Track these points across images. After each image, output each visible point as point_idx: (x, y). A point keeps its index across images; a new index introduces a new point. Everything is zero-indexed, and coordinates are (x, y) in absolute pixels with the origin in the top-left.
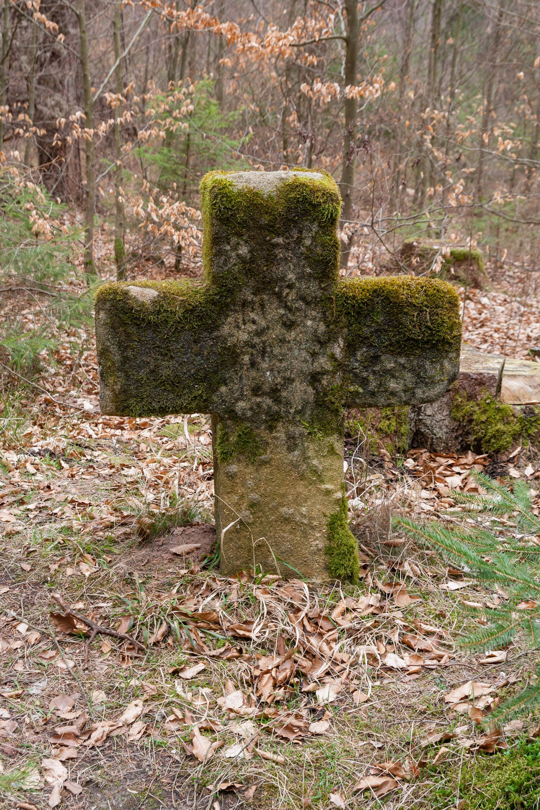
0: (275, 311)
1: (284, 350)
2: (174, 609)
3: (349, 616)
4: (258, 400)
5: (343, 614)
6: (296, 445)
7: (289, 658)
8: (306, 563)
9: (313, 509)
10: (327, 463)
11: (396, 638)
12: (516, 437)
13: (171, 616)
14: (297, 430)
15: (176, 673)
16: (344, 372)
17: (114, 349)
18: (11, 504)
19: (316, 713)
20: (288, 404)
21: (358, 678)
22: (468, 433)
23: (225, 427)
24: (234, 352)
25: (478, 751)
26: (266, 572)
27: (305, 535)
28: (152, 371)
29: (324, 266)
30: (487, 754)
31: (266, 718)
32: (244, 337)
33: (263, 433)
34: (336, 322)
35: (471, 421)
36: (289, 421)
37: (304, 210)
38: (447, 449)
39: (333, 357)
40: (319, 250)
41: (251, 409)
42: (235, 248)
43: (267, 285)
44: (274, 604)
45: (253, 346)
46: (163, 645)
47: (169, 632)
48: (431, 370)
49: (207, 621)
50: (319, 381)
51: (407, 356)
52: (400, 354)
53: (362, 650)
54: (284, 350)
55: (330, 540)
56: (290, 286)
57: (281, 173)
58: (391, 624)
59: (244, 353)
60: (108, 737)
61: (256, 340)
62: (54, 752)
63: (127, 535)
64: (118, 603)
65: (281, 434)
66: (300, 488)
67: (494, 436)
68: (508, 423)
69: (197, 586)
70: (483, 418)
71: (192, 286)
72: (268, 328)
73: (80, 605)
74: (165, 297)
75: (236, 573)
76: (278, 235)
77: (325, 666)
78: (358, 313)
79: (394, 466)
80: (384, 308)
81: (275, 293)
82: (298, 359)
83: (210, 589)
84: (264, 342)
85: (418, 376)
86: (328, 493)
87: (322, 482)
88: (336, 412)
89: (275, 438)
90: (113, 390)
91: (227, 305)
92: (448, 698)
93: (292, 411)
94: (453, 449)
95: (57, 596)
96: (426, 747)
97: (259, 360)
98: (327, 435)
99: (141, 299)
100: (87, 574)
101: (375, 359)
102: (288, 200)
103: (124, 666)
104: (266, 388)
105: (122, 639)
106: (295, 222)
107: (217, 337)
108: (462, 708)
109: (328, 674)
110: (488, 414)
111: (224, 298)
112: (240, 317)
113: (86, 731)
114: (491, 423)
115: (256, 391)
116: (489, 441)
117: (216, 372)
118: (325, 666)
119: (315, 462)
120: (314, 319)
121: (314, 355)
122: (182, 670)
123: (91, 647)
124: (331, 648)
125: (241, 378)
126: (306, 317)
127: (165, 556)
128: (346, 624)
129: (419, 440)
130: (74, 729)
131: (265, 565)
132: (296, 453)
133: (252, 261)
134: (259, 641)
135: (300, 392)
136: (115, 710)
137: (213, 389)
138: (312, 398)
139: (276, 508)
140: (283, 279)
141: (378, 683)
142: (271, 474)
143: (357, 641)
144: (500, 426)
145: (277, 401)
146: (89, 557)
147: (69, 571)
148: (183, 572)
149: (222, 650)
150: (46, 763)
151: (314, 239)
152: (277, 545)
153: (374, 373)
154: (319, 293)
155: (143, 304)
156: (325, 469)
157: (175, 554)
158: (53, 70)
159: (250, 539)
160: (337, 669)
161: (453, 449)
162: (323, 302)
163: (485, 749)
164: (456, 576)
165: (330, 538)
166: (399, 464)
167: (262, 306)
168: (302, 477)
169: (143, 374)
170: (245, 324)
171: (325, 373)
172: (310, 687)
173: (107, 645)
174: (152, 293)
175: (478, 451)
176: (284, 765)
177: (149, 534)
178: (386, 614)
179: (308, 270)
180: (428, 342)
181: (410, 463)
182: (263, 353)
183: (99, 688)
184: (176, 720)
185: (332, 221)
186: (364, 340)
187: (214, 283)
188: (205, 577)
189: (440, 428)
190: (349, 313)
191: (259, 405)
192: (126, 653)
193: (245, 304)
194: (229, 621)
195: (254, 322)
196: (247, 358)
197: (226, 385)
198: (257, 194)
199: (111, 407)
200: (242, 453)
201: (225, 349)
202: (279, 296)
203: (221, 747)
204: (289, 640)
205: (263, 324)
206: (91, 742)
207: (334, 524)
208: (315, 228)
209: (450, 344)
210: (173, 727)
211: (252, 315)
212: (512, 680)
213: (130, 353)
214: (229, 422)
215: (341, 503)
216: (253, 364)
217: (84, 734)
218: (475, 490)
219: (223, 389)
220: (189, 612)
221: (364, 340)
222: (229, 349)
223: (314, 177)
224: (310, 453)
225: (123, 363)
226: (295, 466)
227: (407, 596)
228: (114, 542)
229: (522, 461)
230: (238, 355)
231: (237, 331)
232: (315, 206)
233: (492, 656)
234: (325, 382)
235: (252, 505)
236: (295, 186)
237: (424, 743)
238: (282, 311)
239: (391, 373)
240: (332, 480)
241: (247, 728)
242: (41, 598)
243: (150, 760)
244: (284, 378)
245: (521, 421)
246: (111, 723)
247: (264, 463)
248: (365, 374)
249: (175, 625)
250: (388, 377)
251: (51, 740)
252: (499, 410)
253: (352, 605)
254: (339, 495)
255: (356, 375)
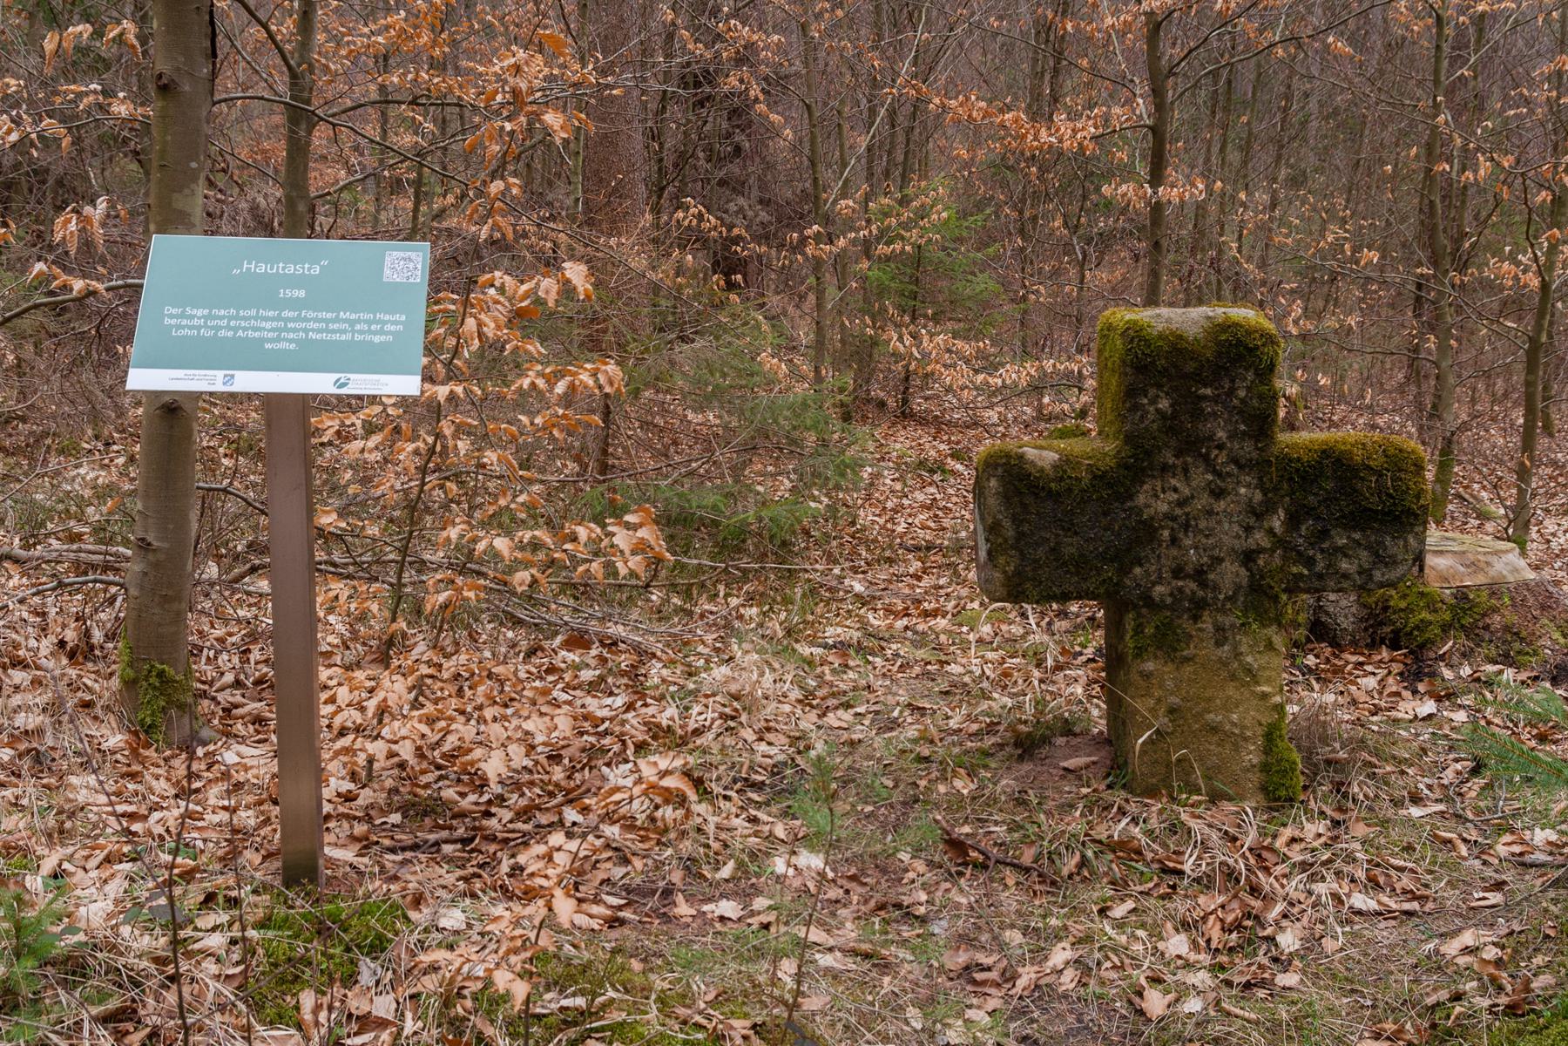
0: (1202, 477)
1: (1213, 523)
2: (1086, 835)
3: (1297, 847)
4: (1180, 583)
5: (1288, 845)
6: (1226, 639)
7: (1235, 896)
8: (1236, 783)
9: (1245, 716)
10: (1264, 660)
11: (1360, 875)
12: (1446, 628)
13: (1083, 844)
14: (1227, 621)
15: (1103, 912)
16: (1285, 549)
17: (1007, 523)
18: (836, 708)
19: (1282, 962)
20: (1216, 588)
21: (1322, 922)
22: (1381, 624)
23: (1139, 615)
24: (1151, 526)
25: (1505, 1013)
26: (1190, 793)
27: (1236, 748)
28: (1053, 550)
29: (1261, 423)
30: (1516, 1015)
31: (1222, 968)
32: (1164, 508)
33: (1185, 623)
34: (1276, 489)
35: (1386, 608)
36: (1218, 610)
37: (1239, 355)
38: (1354, 643)
39: (1271, 531)
40: (1255, 403)
41: (1171, 594)
42: (1153, 402)
43: (1193, 446)
44: (1207, 830)
45: (1174, 519)
46: (1078, 879)
47: (1084, 862)
48: (1392, 546)
49: (1126, 850)
50: (1255, 561)
51: (1363, 530)
52: (1354, 528)
53: (1320, 888)
54: (1213, 523)
55: (1266, 753)
56: (1220, 447)
57: (1219, 312)
58: (1351, 859)
59: (1163, 528)
60: (1037, 987)
61: (1178, 511)
62: (975, 1001)
63: (1001, 746)
64: (1014, 827)
65: (1207, 624)
66: (1231, 691)
67: (1417, 627)
68: (1435, 611)
69: (1105, 809)
70: (1403, 605)
71: (1097, 445)
72: (1193, 497)
73: (967, 829)
74: (1068, 461)
75: (1152, 792)
76: (1205, 386)
77: (1279, 908)
78: (1303, 478)
79: (1293, 665)
80: (1335, 471)
81: (1201, 455)
82: (1229, 534)
83: (1122, 812)
84: (1187, 514)
85: (1377, 555)
86: (1265, 696)
87: (1257, 683)
88: (1276, 599)
89: (1200, 630)
90: (1005, 572)
91: (1143, 470)
92: (1443, 949)
93: (1221, 597)
94: (1362, 644)
95: (939, 817)
96: (1433, 1007)
97: (1181, 535)
98: (1264, 626)
99: (1040, 464)
100: (965, 792)
101: (1324, 534)
102: (1219, 343)
103: (1037, 902)
104: (1189, 569)
105: (1027, 870)
106: (1227, 369)
107: (1131, 508)
108: (1463, 961)
109: (1285, 916)
110: (1409, 599)
111: (1139, 462)
112: (1159, 484)
113: (1010, 977)
114: (1412, 611)
115: (1178, 572)
116: (1411, 633)
117: (1129, 550)
118: (1279, 908)
119: (1249, 659)
120: (1248, 486)
121: (1248, 529)
122: (1108, 908)
123: (992, 880)
124: (1283, 886)
125: (1159, 557)
126: (1238, 483)
127: (1054, 772)
128: (1297, 856)
129: (1321, 631)
130: (994, 975)
131: (1187, 784)
132: (1226, 648)
133: (1174, 416)
134: (1194, 875)
135: (1231, 574)
136: (1039, 955)
137: (1124, 571)
138: (1245, 582)
139: (1201, 715)
140: (1211, 438)
141: (1347, 929)
142: (1195, 673)
143: (1313, 878)
144: (1425, 615)
145: (1203, 584)
146: (962, 771)
147: (942, 789)
148: (1085, 791)
149: (1151, 885)
150: (970, 1014)
151: (1249, 389)
152: (1201, 759)
153: (1322, 551)
154: (1255, 455)
155: (1042, 470)
156: (1262, 668)
157: (1065, 769)
158: (734, 168)
159: (1168, 752)
160: (1295, 910)
161: (1362, 644)
162: (1259, 466)
163: (1512, 1010)
164: (1416, 799)
165: (1267, 751)
166: (1298, 661)
167: (1186, 471)
168: (1233, 677)
169: (1041, 552)
170: (1164, 492)
171: (1260, 551)
172: (1269, 931)
173: (1011, 878)
174: (1051, 457)
175: (1394, 646)
176: (1257, 1023)
177: (1027, 745)
178: (1344, 846)
179: (1243, 427)
180: (1390, 512)
181: (1311, 660)
182: (1186, 527)
183: (1012, 926)
184: (1114, 967)
185: (1272, 367)
186: (1310, 511)
187: (1126, 443)
188: (1118, 797)
189: (1346, 617)
190: (1291, 479)
191: (1180, 590)
192: (1037, 887)
193: (1165, 468)
194: (1153, 850)
195: (1175, 490)
196: (1166, 533)
197: (1141, 565)
198: (1181, 337)
199: (1001, 592)
200: (1159, 648)
201: (1140, 522)
202: (1206, 458)
203: (1177, 1000)
204: (1230, 875)
205: (1187, 491)
206: (1018, 990)
207: (1271, 735)
208: (1250, 376)
209: (1416, 516)
210: (1113, 975)
211: (1173, 482)
212: (1517, 928)
213: (1026, 528)
214: (1144, 611)
215: (1280, 709)
216: (1174, 541)
217: (1006, 981)
218: (1398, 694)
219: (1138, 570)
220: (1103, 837)
221: (1310, 511)
222: (1144, 522)
223: (1244, 314)
224: (1244, 649)
225: (1018, 540)
226: (1224, 663)
227: (1361, 824)
228: (986, 754)
229: (1455, 659)
230: (1156, 530)
231: (1155, 501)
232: (1250, 350)
233: (1484, 898)
234: (1261, 562)
235: (1172, 711)
236: (1228, 326)
237: (1430, 1001)
238: (1210, 477)
239: (1343, 551)
240: (1269, 681)
241: (1201, 978)
242: (915, 819)
243: (1093, 1013)
244: (1211, 558)
245: (1452, 608)
246: (1036, 968)
247: (1187, 660)
248: (1311, 553)
249: (1090, 854)
250: (1340, 556)
251: (969, 988)
252: (1422, 594)
253: (1297, 834)
254: (1278, 699)
255: (1299, 553)
